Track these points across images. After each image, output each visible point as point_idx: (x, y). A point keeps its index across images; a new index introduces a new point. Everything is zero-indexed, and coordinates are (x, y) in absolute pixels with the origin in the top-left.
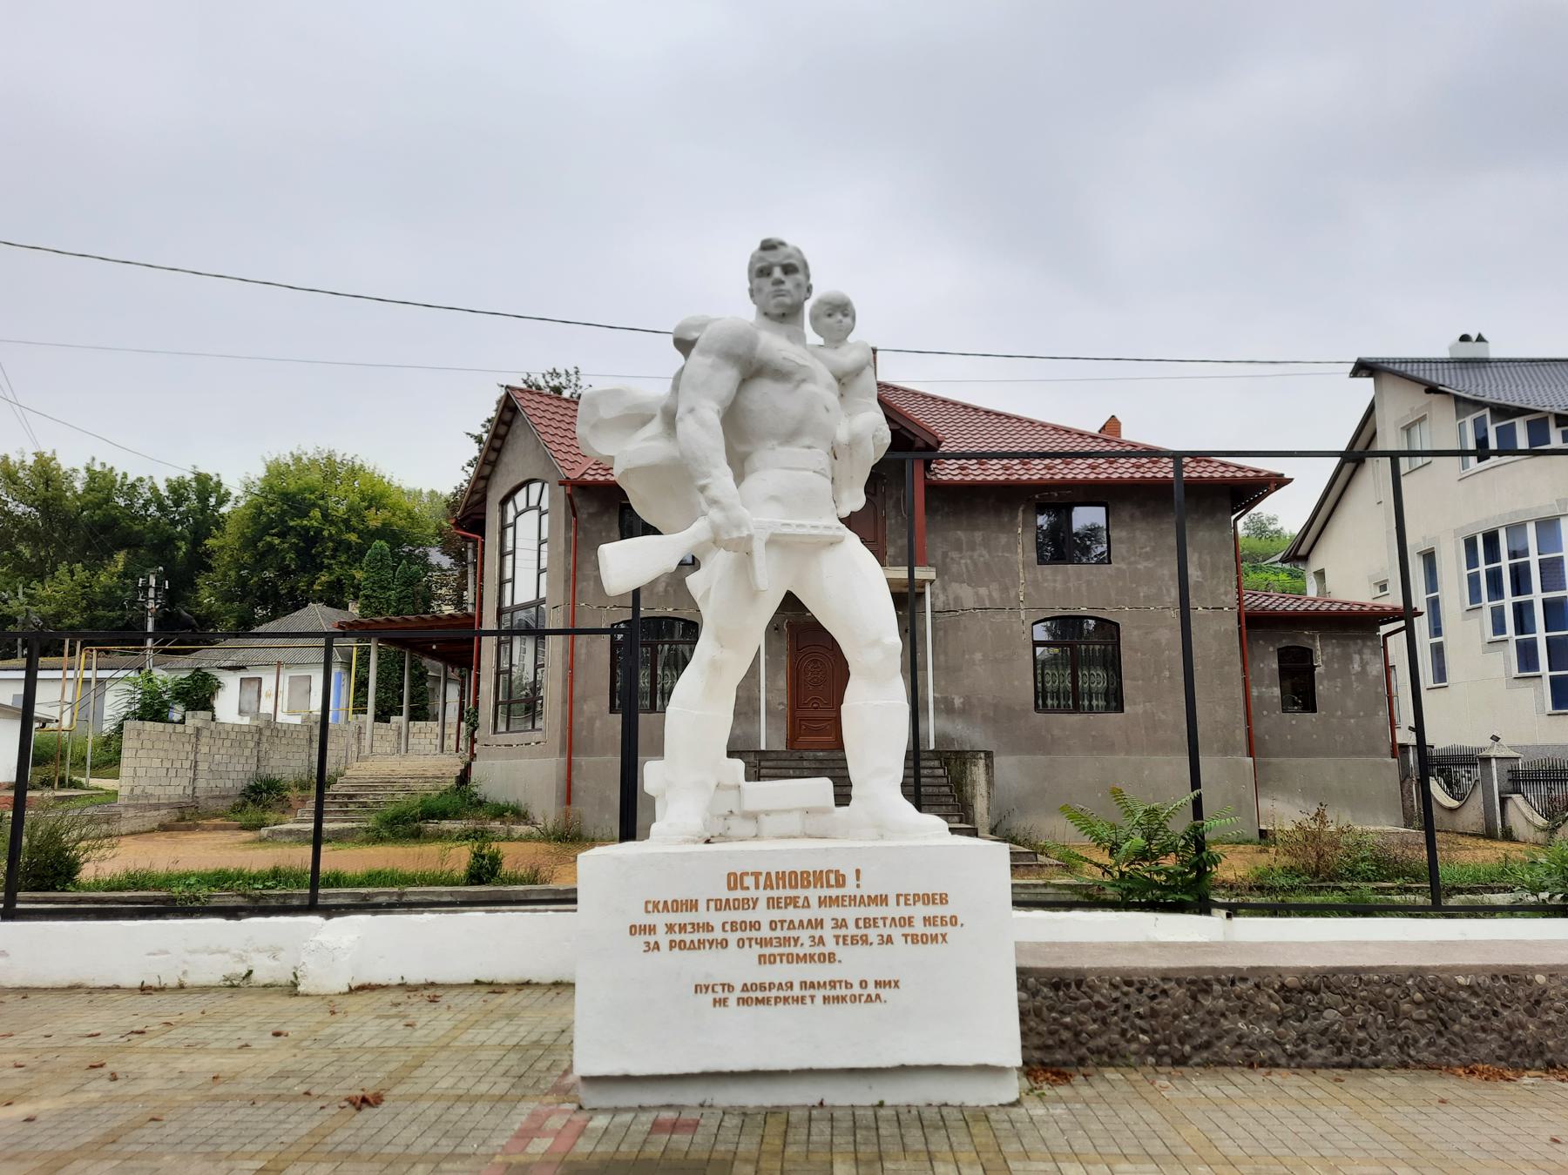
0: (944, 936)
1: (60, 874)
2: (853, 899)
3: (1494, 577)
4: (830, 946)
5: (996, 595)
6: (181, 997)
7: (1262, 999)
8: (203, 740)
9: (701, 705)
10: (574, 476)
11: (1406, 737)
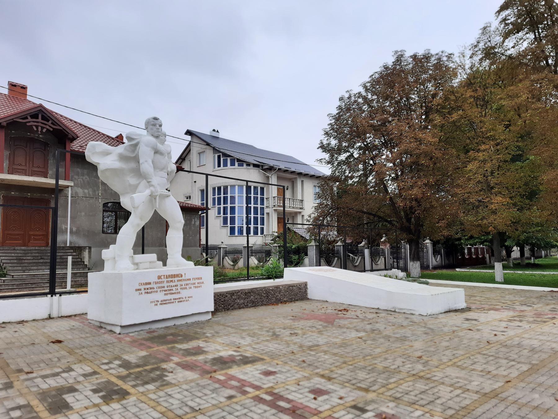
3: (219, 199)
4: (179, 290)
5: (91, 193)
7: (242, 296)
9: (128, 232)
11: (203, 242)
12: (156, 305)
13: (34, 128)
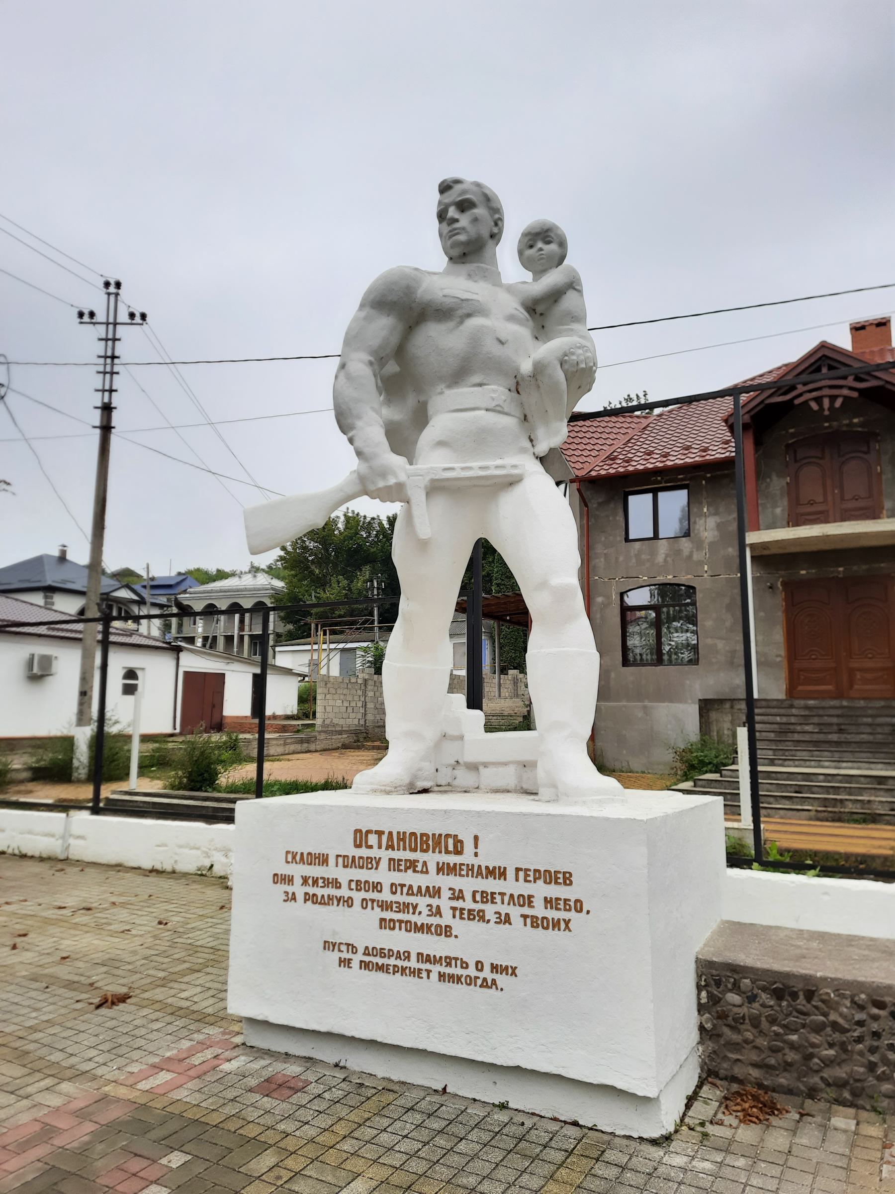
0: (567, 922)
1: (205, 780)
2: (470, 868)
4: (447, 919)
6: (153, 879)
8: (369, 687)
10: (580, 473)
12: (345, 963)
13: (814, 406)
